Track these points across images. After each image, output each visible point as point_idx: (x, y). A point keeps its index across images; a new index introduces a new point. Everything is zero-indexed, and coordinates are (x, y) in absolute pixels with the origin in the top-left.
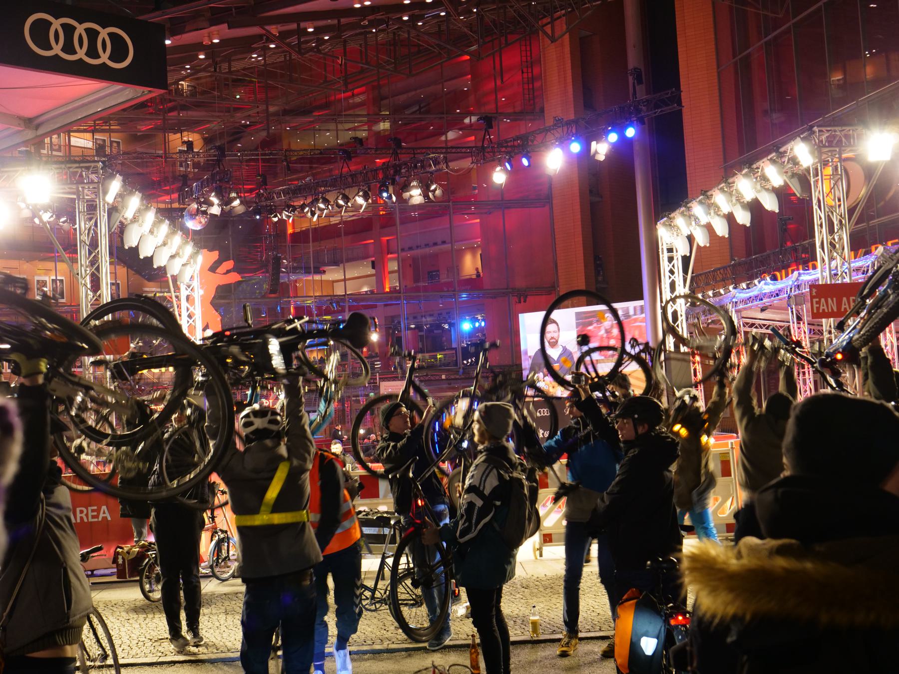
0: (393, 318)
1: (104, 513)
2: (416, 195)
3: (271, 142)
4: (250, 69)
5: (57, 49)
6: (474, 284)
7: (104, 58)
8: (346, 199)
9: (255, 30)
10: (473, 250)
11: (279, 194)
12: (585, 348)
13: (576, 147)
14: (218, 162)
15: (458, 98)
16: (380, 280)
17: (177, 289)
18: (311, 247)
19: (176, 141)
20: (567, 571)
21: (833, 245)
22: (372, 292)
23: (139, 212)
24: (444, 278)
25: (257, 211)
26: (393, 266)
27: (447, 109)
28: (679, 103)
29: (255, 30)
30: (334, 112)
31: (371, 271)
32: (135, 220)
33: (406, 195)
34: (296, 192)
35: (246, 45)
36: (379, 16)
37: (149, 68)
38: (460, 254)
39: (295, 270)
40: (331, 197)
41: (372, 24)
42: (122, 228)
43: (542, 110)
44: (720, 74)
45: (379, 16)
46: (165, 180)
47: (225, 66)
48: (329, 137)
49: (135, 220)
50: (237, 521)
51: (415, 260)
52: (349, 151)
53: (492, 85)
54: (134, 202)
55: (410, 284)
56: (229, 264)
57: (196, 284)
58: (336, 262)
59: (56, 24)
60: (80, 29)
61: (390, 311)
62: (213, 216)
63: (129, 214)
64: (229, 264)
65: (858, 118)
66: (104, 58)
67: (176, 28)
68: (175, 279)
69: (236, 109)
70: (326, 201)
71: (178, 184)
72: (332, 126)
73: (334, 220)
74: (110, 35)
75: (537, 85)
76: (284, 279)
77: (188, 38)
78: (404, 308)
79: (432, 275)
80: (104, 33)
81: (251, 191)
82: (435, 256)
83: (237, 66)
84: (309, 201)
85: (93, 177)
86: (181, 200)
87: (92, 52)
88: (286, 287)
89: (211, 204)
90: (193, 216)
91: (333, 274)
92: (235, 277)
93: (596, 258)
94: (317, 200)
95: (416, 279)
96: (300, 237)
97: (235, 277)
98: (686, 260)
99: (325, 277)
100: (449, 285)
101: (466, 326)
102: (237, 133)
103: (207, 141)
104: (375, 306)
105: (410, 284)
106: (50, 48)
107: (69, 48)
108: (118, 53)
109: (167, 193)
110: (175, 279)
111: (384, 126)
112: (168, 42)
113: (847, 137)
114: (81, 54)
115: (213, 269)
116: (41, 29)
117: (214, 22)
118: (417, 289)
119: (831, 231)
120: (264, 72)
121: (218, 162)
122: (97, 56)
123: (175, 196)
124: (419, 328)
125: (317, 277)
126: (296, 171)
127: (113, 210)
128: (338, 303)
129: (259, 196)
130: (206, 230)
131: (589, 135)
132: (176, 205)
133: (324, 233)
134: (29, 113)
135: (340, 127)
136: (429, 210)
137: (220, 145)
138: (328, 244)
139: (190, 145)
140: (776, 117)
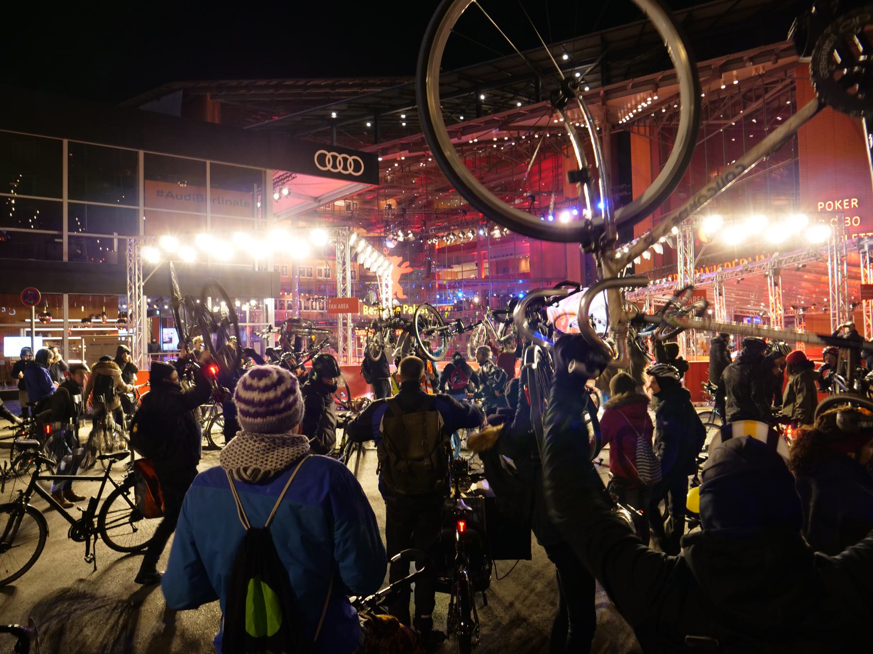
0: (485, 291)
2: (497, 233)
3: (429, 204)
4: (421, 170)
5: (329, 167)
6: (525, 276)
7: (350, 171)
8: (463, 234)
9: (422, 153)
10: (526, 259)
12: (792, 86)
13: (575, 212)
14: (402, 215)
16: (480, 273)
17: (381, 281)
18: (446, 255)
19: (384, 204)
23: (365, 248)
24: (511, 272)
26: (486, 265)
28: (631, 191)
29: (422, 153)
31: (475, 267)
32: (362, 251)
33: (492, 233)
34: (442, 229)
35: (418, 159)
36: (482, 146)
38: (519, 260)
39: (438, 266)
40: (456, 233)
41: (478, 149)
42: (356, 255)
43: (562, 191)
46: (377, 222)
47: (407, 169)
49: (362, 251)
51: (497, 263)
54: (363, 243)
55: (495, 274)
56: (407, 264)
57: (390, 278)
58: (458, 263)
59: (329, 155)
60: (340, 157)
62: (400, 242)
66: (350, 171)
67: (384, 152)
69: (413, 189)
70: (454, 235)
71: (385, 224)
73: (458, 243)
74: (354, 160)
75: (560, 178)
76: (433, 270)
77: (390, 157)
78: (491, 286)
79: (505, 270)
80: (350, 159)
81: (418, 228)
82: (507, 261)
83: (413, 168)
86: (385, 231)
88: (434, 274)
89: (398, 236)
90: (390, 240)
91: (457, 269)
92: (409, 270)
93: (587, 264)
95: (497, 272)
96: (442, 250)
97: (409, 270)
100: (513, 275)
102: (413, 200)
105: (495, 274)
108: (357, 168)
109: (379, 228)
114: (340, 169)
115: (399, 266)
116: (322, 158)
118: (497, 277)
120: (426, 171)
121: (402, 215)
122: (347, 170)
123: (383, 230)
124: (498, 296)
125: (449, 270)
126: (440, 218)
127: (352, 248)
129: (422, 231)
130: (397, 247)
132: (383, 235)
137: (405, 204)
138: (454, 255)
139: (390, 206)
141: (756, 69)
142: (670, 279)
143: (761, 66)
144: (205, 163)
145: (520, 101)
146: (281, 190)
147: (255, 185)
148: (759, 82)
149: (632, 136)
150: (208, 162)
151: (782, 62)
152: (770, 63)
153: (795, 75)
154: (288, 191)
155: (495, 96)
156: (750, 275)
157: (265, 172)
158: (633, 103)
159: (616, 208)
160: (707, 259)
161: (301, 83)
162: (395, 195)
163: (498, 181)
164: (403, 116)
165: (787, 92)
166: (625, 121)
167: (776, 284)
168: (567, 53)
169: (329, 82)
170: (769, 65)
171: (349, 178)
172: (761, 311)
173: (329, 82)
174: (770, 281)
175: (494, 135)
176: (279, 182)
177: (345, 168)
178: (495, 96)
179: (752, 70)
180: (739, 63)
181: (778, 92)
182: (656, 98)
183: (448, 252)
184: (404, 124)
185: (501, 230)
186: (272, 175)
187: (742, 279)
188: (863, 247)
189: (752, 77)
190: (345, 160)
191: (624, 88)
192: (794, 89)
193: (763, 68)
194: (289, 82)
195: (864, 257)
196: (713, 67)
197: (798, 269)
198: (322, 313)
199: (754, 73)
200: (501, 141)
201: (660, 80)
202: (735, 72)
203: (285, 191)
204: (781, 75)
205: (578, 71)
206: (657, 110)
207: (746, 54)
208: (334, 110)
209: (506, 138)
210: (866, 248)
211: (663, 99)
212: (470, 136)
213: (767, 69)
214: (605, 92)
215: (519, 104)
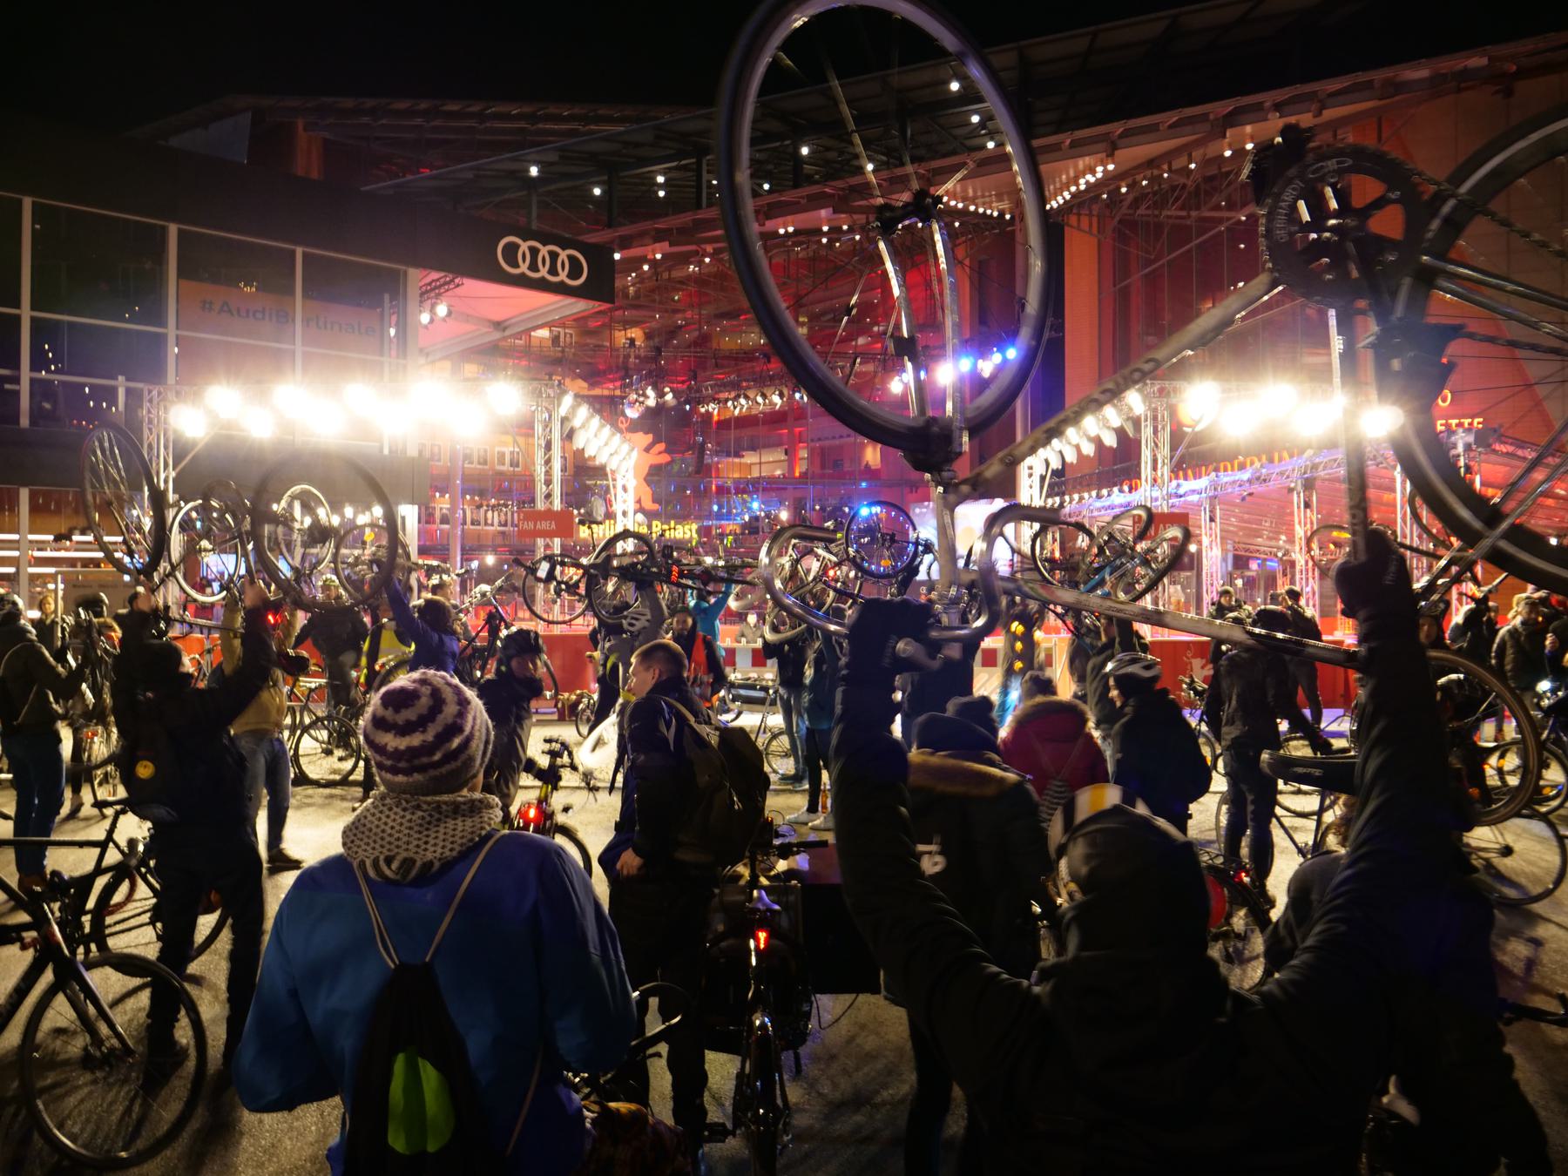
3: (704, 340)
4: (691, 278)
5: (524, 268)
7: (563, 276)
8: (764, 396)
16: (791, 468)
18: (733, 434)
19: (621, 337)
20: (44, 856)
21: (1155, 480)
23: (588, 420)
24: (847, 467)
25: (688, 402)
26: (804, 454)
31: (783, 457)
32: (583, 426)
35: (685, 259)
36: (801, 238)
37: (600, 285)
39: (717, 453)
40: (751, 394)
44: (1100, 301)
51: (822, 449)
54: (584, 411)
55: (818, 471)
57: (630, 475)
59: (524, 246)
60: (544, 251)
61: (799, 494)
63: (576, 423)
64: (661, 447)
65: (1180, 370)
66: (563, 276)
67: (624, 244)
68: (613, 472)
70: (747, 397)
73: (754, 412)
76: (707, 460)
77: (635, 252)
79: (837, 464)
80: (563, 255)
81: (683, 382)
82: (841, 447)
84: (733, 395)
85: (551, 392)
86: (623, 387)
87: (553, 271)
88: (709, 467)
89: (647, 397)
90: (632, 404)
91: (750, 458)
92: (665, 458)
95: (823, 467)
96: (724, 424)
97: (665, 458)
98: (1043, 478)
100: (851, 474)
101: (864, 511)
102: (673, 332)
103: (648, 336)
106: (518, 266)
107: (534, 267)
108: (575, 272)
109: (613, 381)
110: (613, 472)
112: (617, 256)
113: (1175, 390)
114: (543, 272)
115: (647, 450)
116: (511, 251)
117: (657, 239)
118: (822, 476)
119: (1155, 468)
120: (698, 280)
123: (618, 384)
125: (737, 460)
126: (723, 367)
127: (564, 420)
129: (690, 388)
130: (642, 417)
131: (982, 350)
132: (618, 393)
133: (745, 422)
134: (497, 318)
137: (661, 339)
138: (748, 432)
139: (632, 341)
140: (1151, 339)
147: (387, 297)
150: (299, 251)
151: (1329, 114)
154: (444, 310)
155: (828, 149)
157: (405, 273)
158: (1072, 173)
160: (1191, 456)
163: (828, 304)
167: (1307, 505)
169: (527, 109)
171: (561, 289)
172: (1279, 548)
173: (527, 109)
175: (823, 218)
176: (430, 293)
180: (1256, 113)
186: (417, 278)
194: (453, 107)
196: (1212, 117)
198: (503, 533)
201: (1121, 136)
202: (1248, 129)
203: (442, 310)
205: (976, 112)
207: (1268, 98)
208: (536, 163)
211: (1124, 168)
212: (780, 220)
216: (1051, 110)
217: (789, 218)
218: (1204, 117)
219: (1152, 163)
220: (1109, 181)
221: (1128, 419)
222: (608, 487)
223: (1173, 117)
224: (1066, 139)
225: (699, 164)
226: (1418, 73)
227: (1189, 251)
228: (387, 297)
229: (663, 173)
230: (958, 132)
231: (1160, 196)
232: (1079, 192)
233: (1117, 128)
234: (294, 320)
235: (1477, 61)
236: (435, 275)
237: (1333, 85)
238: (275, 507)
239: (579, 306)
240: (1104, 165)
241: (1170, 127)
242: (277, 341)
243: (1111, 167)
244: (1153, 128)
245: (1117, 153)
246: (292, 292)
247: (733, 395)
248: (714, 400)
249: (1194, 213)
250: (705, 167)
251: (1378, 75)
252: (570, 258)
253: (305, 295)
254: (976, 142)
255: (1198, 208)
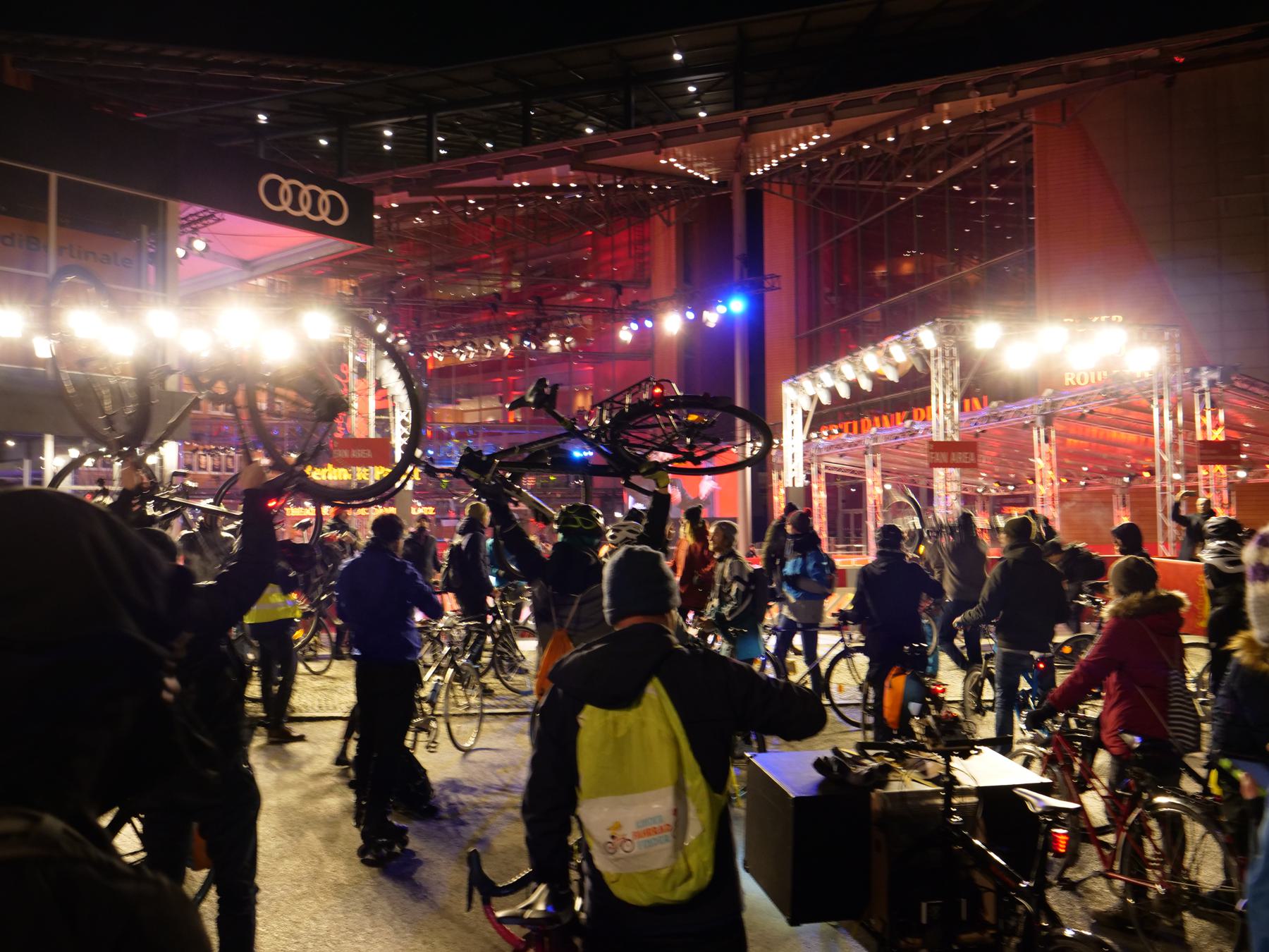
1: (674, 568)
2: (554, 345)
3: (419, 292)
4: (417, 230)
5: (285, 206)
7: (324, 216)
8: (492, 344)
10: (584, 392)
11: (431, 337)
15: (579, 266)
18: (453, 380)
22: (496, 422)
27: (567, 274)
29: (430, 199)
30: (478, 271)
33: (546, 344)
44: (797, 262)
45: (530, 195)
48: (470, 291)
50: (852, 570)
52: (492, 304)
53: (609, 257)
59: (286, 184)
60: (306, 190)
66: (324, 216)
72: (476, 282)
80: (324, 195)
83: (403, 226)
84: (459, 342)
91: (466, 405)
94: (465, 344)
98: (805, 413)
99: (461, 408)
104: (500, 434)
107: (295, 206)
108: (336, 212)
111: (516, 285)
113: (962, 328)
114: (305, 211)
116: (273, 188)
117: (396, 189)
118: (540, 422)
125: (450, 407)
128: (473, 429)
135: (484, 283)
136: (565, 355)
141: (982, 103)
142: (825, 433)
143: (988, 98)
144: (46, 178)
145: (591, 126)
146: (191, 240)
147: (144, 228)
148: (979, 126)
149: (766, 196)
150: (53, 176)
151: (1023, 94)
152: (1005, 95)
153: (1033, 118)
154: (207, 242)
155: (551, 112)
156: (1001, 424)
157: (165, 204)
158: (782, 143)
159: (295, 390)
160: (978, 386)
161: (194, 56)
162: (362, 271)
163: (541, 260)
164: (388, 133)
165: (1019, 143)
166: (760, 171)
167: (1047, 440)
168: (681, 52)
169: (249, 59)
170: (1003, 98)
171: (321, 228)
172: (979, 485)
173: (249, 59)
174: (1037, 435)
175: (556, 175)
176: (192, 226)
177: (314, 211)
178: (551, 112)
179: (976, 103)
180: (958, 91)
181: (1004, 143)
182: (826, 136)
183: (457, 375)
184: (387, 147)
185: (563, 340)
186: (182, 209)
187: (1091, 412)
188: (1198, 383)
189: (975, 115)
190: (315, 195)
191: (778, 116)
192: (1029, 140)
193: (993, 101)
194: (173, 52)
195: (1202, 398)
196: (919, 93)
197: (1082, 416)
198: (217, 478)
199: (978, 109)
200: (565, 188)
201: (838, 108)
202: (946, 106)
203: (199, 245)
204: (1015, 116)
205: (692, 83)
206: (834, 151)
207: (970, 78)
208: (264, 112)
209: (573, 185)
210: (1205, 385)
211: (840, 135)
212: (515, 175)
213: (999, 104)
214: (749, 118)
215: (589, 131)
216: (764, 82)
217: (524, 173)
218: (912, 93)
219: (858, 135)
220: (822, 147)
221: (917, 355)
222: (388, 421)
223: (885, 91)
224: (790, 108)
225: (429, 120)
226: (1099, 60)
227: (881, 217)
228: (144, 228)
229: (392, 128)
230: (679, 100)
231: (861, 164)
232: (789, 159)
233: (835, 100)
234: (46, 247)
235: (1150, 52)
236: (198, 208)
237: (1027, 69)
238: (506, 353)
239: (334, 246)
240: (819, 133)
241: (883, 101)
242: (29, 268)
243: (826, 136)
244: (866, 102)
245: (834, 123)
246: (44, 219)
247: (459, 342)
248: (439, 348)
249: (888, 184)
250: (435, 125)
251: (1065, 62)
252: (331, 198)
253: (60, 224)
254: (690, 111)
255: (889, 178)
